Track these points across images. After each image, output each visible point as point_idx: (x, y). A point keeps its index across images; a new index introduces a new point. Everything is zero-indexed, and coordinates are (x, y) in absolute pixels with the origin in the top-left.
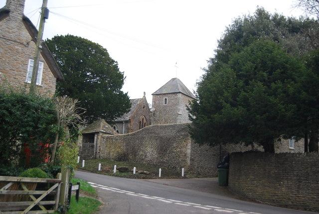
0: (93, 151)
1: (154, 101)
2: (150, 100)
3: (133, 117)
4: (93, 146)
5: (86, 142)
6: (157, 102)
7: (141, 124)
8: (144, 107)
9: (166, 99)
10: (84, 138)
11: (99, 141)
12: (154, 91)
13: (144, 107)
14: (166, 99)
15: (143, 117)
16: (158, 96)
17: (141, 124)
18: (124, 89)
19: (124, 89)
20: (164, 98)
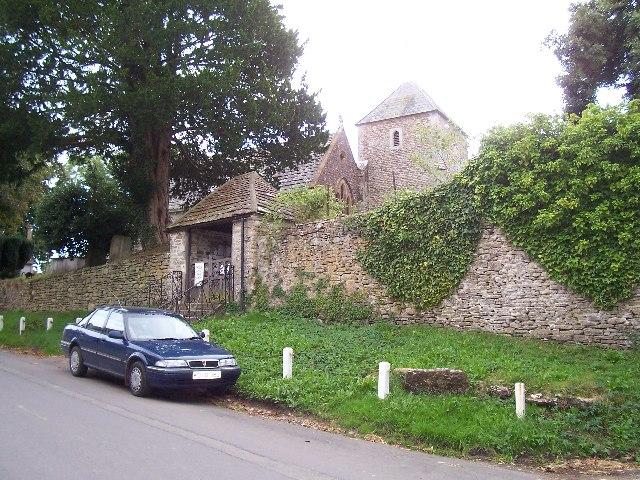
6: (372, 143)
9: (396, 133)
11: (249, 245)
12: (358, 118)
14: (396, 133)
15: (343, 181)
16: (374, 128)
20: (392, 131)
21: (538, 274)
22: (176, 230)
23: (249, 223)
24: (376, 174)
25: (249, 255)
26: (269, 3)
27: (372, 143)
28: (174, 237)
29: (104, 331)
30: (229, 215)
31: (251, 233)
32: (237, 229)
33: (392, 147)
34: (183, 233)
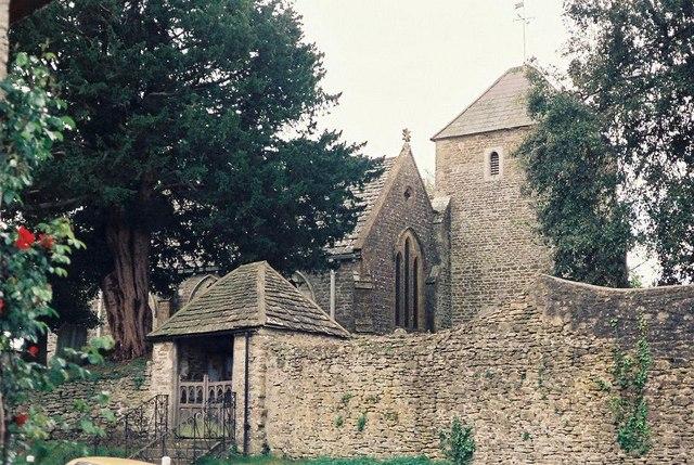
0: (232, 421)
1: (444, 168)
2: (427, 163)
3: (372, 239)
4: (227, 398)
5: (195, 375)
6: (457, 169)
7: (403, 264)
8: (407, 195)
9: (494, 155)
10: (180, 357)
11: (255, 368)
12: (436, 127)
13: (407, 195)
14: (494, 155)
15: (408, 234)
16: (461, 145)
17: (403, 264)
18: (305, 40)
19: (305, 40)
20: (488, 152)
21: (570, 428)
22: (162, 339)
23: (255, 339)
24: (463, 218)
25: (254, 380)
26: (286, 73)
27: (457, 169)
28: (157, 348)
29: (247, 427)
30: (230, 326)
31: (256, 351)
32: (239, 344)
33: (487, 177)
34: (170, 344)
